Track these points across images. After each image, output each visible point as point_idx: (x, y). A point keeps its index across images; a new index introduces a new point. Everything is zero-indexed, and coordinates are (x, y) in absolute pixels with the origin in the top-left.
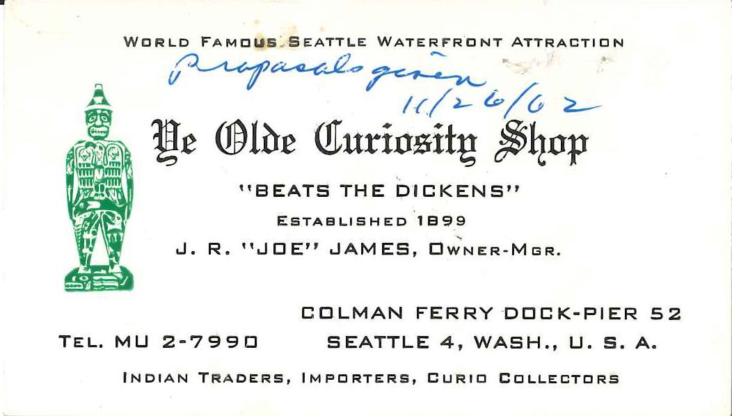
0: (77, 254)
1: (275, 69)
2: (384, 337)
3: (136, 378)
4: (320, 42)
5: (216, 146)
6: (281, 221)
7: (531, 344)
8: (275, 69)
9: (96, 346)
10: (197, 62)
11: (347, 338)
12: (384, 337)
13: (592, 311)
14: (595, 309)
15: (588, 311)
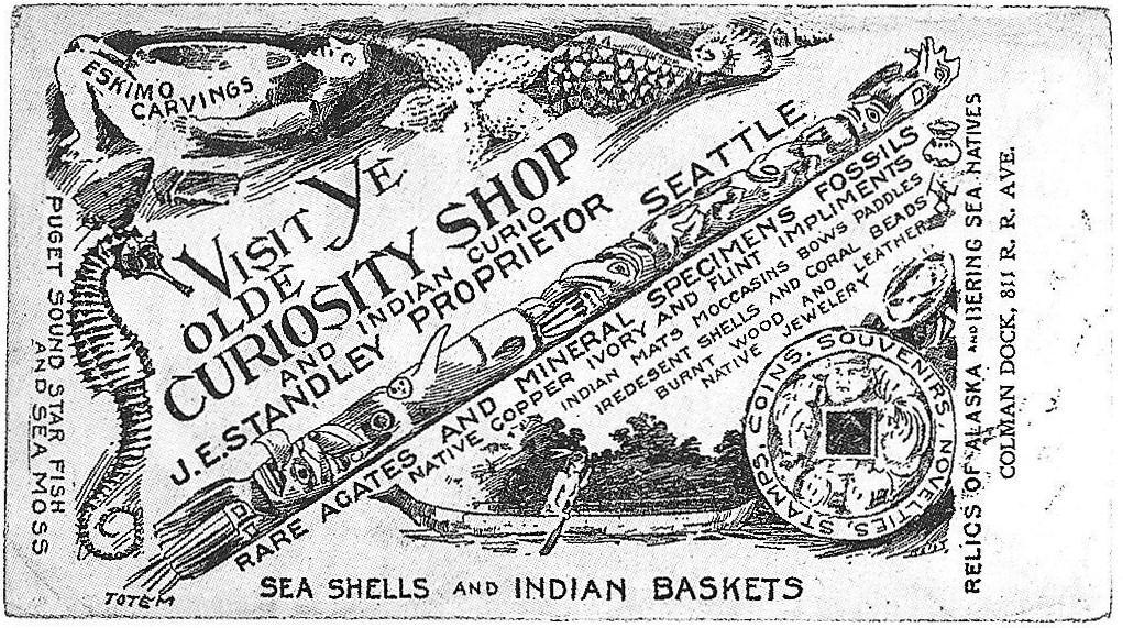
0: (325, 17)
1: (648, 198)
2: (726, 144)
3: (467, 419)
4: (699, 172)
5: (163, 396)
6: (752, 586)
7: (716, 155)
8: (648, 198)
9: (733, 140)
10: (97, 554)
11: (668, 181)
12: (726, 144)
13: (524, 404)
14: (539, 392)
15: (535, 398)
